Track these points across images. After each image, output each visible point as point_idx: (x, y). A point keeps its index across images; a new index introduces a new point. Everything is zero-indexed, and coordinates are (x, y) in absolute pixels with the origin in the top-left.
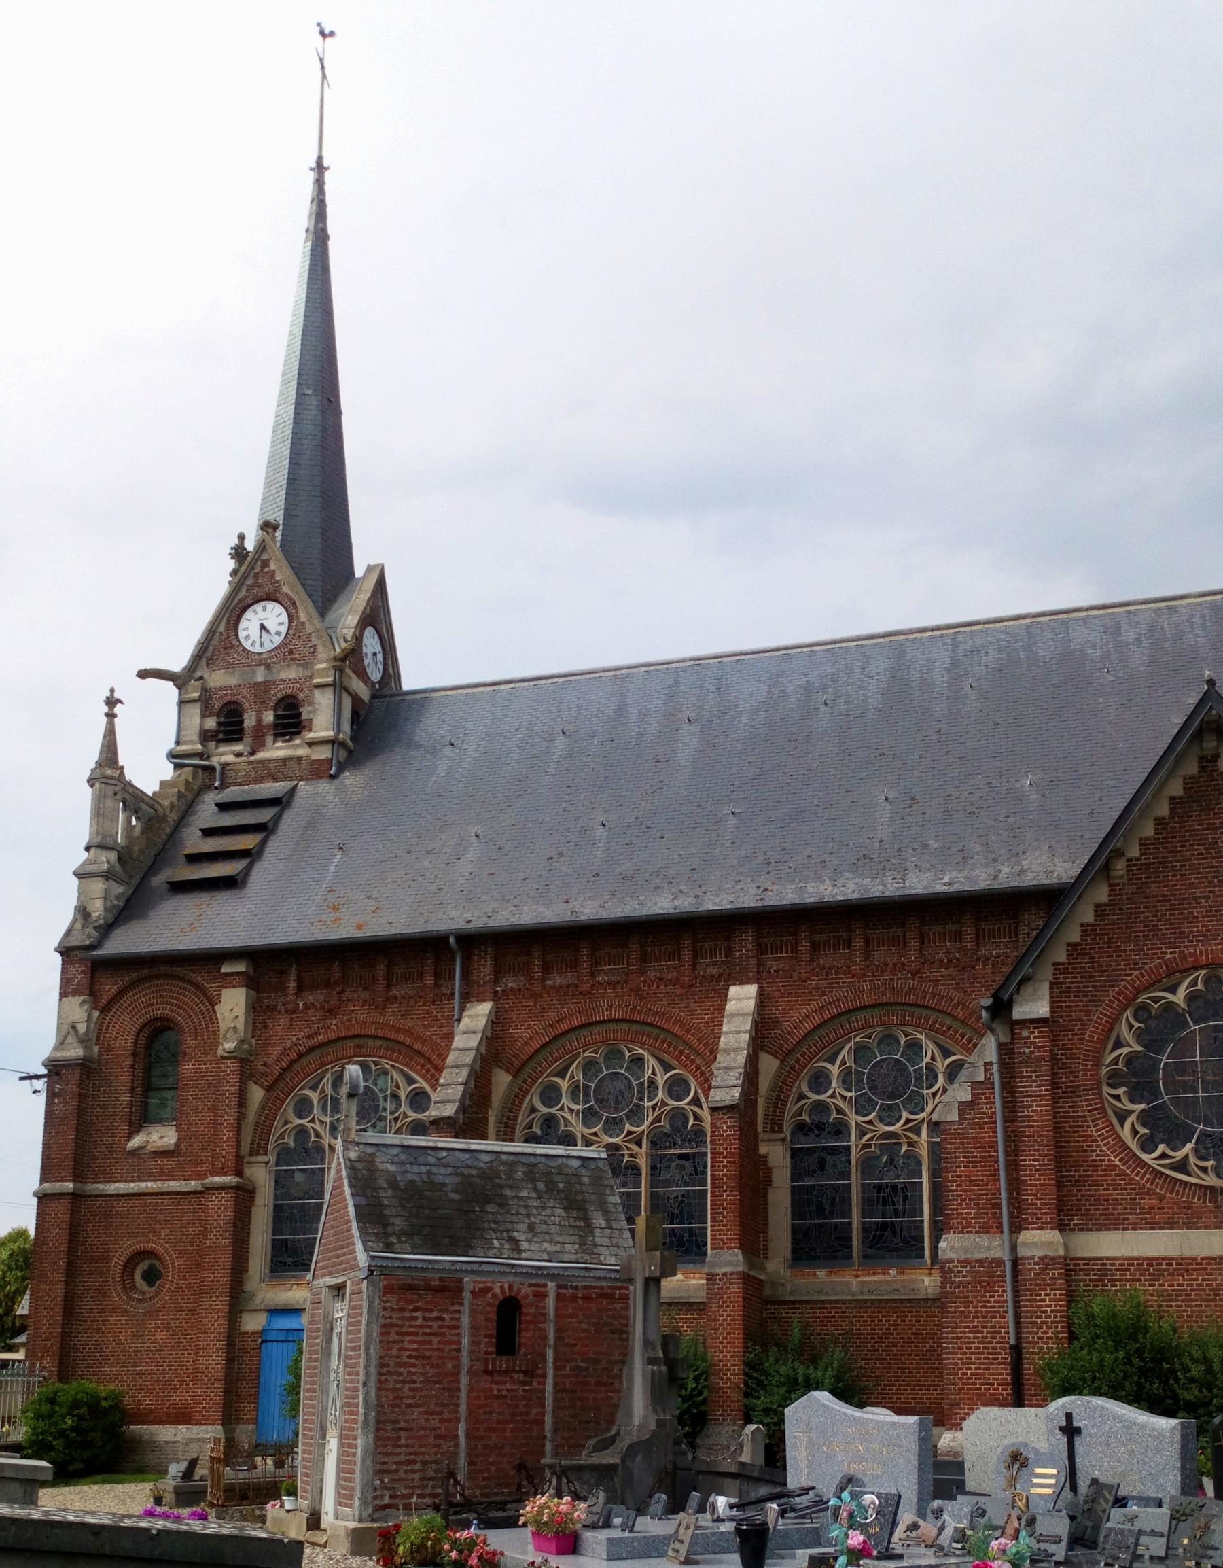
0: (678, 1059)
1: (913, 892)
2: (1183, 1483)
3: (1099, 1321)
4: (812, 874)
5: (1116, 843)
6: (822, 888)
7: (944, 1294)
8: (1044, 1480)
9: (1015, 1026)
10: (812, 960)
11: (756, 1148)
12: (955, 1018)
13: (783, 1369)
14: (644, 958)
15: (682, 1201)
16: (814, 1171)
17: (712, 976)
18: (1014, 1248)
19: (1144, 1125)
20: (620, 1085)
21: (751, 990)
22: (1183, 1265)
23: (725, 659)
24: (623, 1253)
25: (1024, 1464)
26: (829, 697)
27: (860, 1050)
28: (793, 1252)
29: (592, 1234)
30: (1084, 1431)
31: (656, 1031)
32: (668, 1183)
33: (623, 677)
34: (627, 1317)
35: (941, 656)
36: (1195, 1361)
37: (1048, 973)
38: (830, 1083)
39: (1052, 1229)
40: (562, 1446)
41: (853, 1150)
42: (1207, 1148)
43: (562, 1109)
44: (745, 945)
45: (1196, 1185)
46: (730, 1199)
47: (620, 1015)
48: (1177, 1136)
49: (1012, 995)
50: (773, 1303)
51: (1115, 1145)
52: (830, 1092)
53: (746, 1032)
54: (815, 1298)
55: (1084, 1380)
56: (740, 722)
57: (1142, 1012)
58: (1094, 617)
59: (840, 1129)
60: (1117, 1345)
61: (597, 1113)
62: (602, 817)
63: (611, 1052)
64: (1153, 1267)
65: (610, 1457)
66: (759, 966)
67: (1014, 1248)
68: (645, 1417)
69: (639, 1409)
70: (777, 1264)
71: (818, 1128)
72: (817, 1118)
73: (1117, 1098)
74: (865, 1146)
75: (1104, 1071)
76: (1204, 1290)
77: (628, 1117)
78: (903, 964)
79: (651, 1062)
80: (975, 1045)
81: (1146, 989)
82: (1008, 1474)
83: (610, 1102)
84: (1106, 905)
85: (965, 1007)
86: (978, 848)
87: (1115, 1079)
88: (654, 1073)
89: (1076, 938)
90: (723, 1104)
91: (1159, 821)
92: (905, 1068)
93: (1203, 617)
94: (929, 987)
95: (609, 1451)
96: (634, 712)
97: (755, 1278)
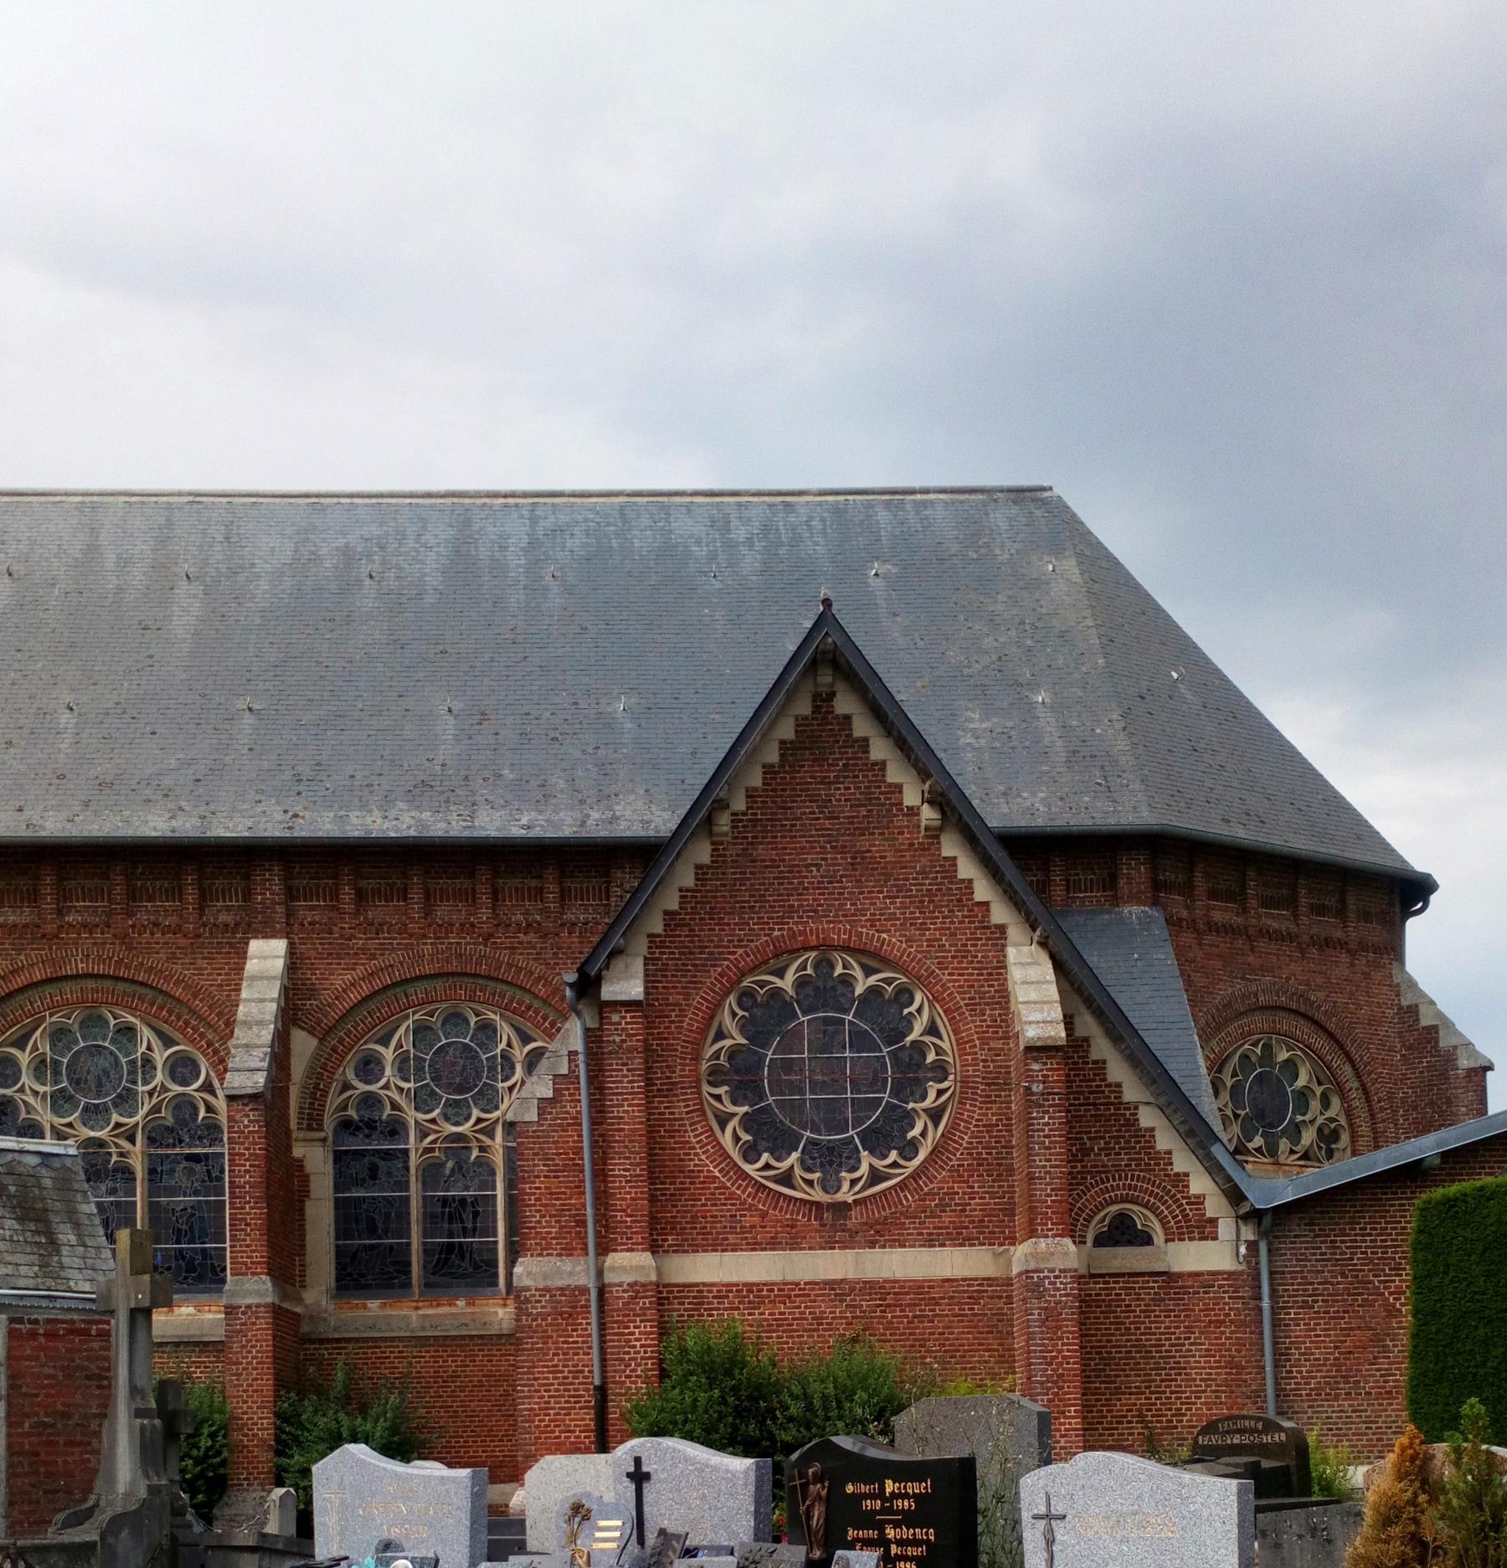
0: (182, 1031)
1: (484, 834)
2: (757, 1529)
3: (693, 1356)
4: (356, 801)
5: (719, 792)
6: (369, 820)
7: (519, 1328)
8: (608, 1533)
9: (605, 1008)
10: (357, 913)
11: (289, 1148)
12: (536, 996)
13: (322, 1422)
14: (133, 895)
15: (192, 1215)
16: (363, 1180)
17: (226, 925)
18: (600, 1273)
19: (747, 1131)
20: (104, 1062)
21: (279, 946)
22: (786, 1291)
23: (236, 500)
24: (101, 1278)
25: (586, 1517)
26: (376, 567)
27: (421, 1030)
28: (338, 1279)
29: (58, 1252)
30: (654, 1477)
31: (150, 994)
32: (172, 1191)
33: (94, 507)
34: (107, 1359)
35: (517, 530)
36: (794, 1397)
37: (641, 946)
38: (382, 1070)
39: (643, 1250)
40: (21, 1523)
41: (412, 1155)
42: (813, 1159)
43: (22, 1090)
44: (269, 888)
45: (801, 1200)
46: (254, 1212)
47: (101, 969)
48: (782, 1143)
49: (600, 970)
50: (313, 1341)
52: (383, 1082)
53: (272, 1000)
54: (366, 1335)
55: (675, 1423)
56: (257, 587)
57: (746, 998)
58: (700, 505)
59: (396, 1129)
60: (712, 1383)
61: (71, 1097)
62: (68, 698)
63: (90, 1017)
64: (753, 1294)
65: (86, 1534)
66: (288, 915)
67: (600, 1273)
68: (133, 1482)
69: (124, 1473)
70: (318, 1293)
71: (370, 1126)
72: (367, 1115)
73: (718, 1098)
74: (427, 1150)
75: (704, 1066)
77: (116, 1105)
78: (473, 925)
79: (146, 1034)
80: (559, 1030)
81: (752, 970)
82: (568, 1530)
83: (87, 1084)
84: (709, 867)
85: (547, 983)
86: (562, 784)
87: (716, 1076)
88: (149, 1048)
90: (243, 1092)
91: (768, 769)
92: (476, 1056)
93: (823, 520)
94: (505, 956)
95: (86, 1525)
96: (110, 557)
97: (287, 1311)
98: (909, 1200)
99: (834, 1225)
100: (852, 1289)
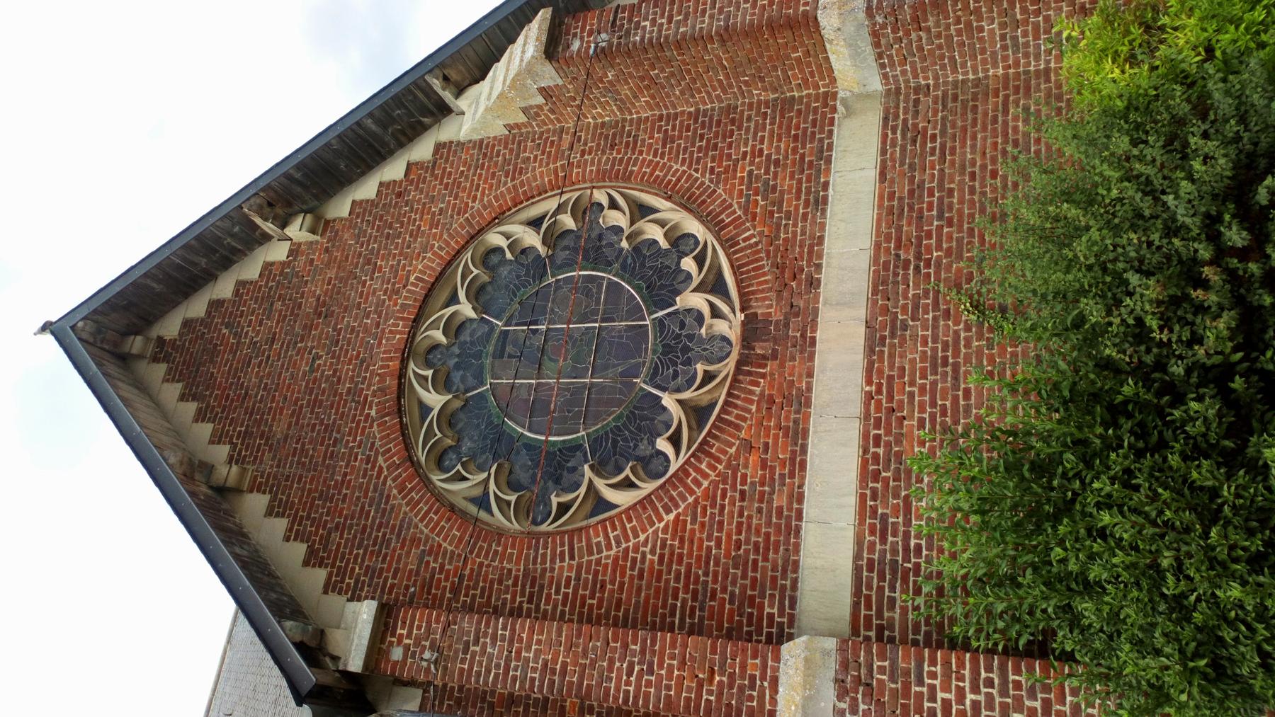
39: (777, 658)
48: (646, 416)
51: (639, 518)
64: (880, 471)
76: (934, 383)
81: (408, 447)
89: (300, 549)
91: (200, 417)
98: (751, 234)
99: (778, 339)
100: (885, 310)
